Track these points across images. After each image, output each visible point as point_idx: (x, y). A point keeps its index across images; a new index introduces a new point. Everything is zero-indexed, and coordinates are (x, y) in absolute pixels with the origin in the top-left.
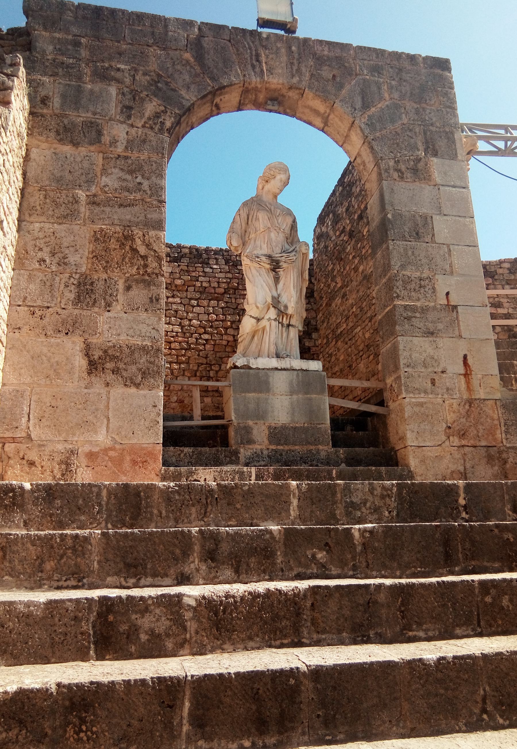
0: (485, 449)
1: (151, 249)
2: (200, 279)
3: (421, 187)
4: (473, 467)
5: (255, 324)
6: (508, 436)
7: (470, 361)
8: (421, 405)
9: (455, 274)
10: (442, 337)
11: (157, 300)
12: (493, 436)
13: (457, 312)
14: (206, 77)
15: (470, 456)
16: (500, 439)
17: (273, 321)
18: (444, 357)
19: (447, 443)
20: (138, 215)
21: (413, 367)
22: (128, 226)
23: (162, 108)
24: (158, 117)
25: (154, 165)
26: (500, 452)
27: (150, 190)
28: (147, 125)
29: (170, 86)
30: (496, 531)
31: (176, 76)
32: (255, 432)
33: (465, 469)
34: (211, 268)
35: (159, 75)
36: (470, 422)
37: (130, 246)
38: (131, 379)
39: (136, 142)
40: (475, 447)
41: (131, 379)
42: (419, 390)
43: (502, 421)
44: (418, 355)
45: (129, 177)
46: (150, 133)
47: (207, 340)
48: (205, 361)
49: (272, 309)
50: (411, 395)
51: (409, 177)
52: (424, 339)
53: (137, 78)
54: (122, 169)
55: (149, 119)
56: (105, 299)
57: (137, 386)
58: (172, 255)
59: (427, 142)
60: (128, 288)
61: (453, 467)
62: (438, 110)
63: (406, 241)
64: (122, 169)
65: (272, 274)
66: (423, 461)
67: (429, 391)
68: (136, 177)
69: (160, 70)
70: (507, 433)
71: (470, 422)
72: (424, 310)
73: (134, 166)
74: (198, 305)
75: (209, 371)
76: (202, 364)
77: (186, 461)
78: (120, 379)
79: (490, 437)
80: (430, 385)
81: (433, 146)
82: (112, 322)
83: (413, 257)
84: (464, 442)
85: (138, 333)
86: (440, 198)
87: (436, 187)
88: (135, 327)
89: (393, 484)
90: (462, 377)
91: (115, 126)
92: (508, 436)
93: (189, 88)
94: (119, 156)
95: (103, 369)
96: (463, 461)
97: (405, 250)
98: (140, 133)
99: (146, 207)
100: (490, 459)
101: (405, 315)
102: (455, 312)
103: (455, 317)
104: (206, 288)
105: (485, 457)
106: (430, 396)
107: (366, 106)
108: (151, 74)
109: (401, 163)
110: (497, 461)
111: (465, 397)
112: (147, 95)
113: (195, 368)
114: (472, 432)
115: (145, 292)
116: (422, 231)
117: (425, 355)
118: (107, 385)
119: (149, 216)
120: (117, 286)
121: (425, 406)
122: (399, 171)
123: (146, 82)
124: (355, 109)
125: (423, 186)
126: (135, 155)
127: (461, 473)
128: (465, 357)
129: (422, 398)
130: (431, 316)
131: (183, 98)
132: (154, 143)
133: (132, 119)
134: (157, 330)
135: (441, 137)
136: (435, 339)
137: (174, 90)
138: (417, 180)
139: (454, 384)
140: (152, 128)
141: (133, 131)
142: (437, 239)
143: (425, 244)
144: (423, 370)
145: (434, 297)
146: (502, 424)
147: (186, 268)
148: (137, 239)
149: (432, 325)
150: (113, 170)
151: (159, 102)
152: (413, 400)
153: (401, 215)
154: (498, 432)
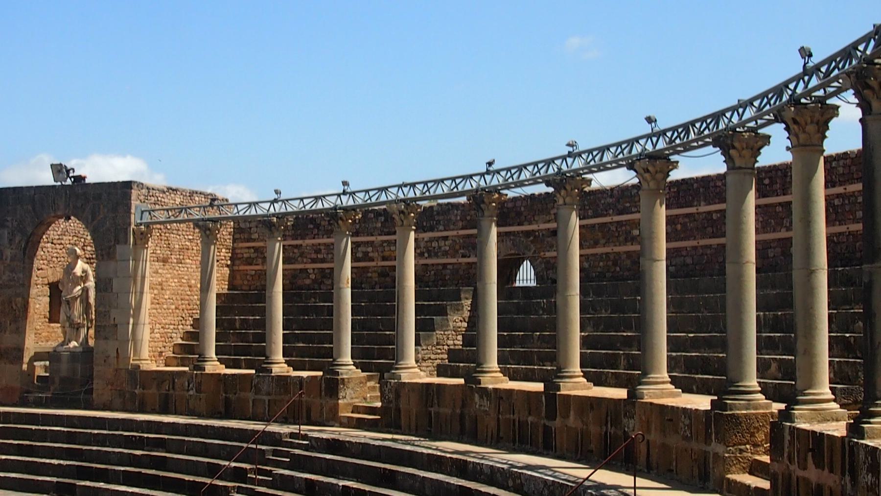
107: (93, 220)
122: (102, 255)
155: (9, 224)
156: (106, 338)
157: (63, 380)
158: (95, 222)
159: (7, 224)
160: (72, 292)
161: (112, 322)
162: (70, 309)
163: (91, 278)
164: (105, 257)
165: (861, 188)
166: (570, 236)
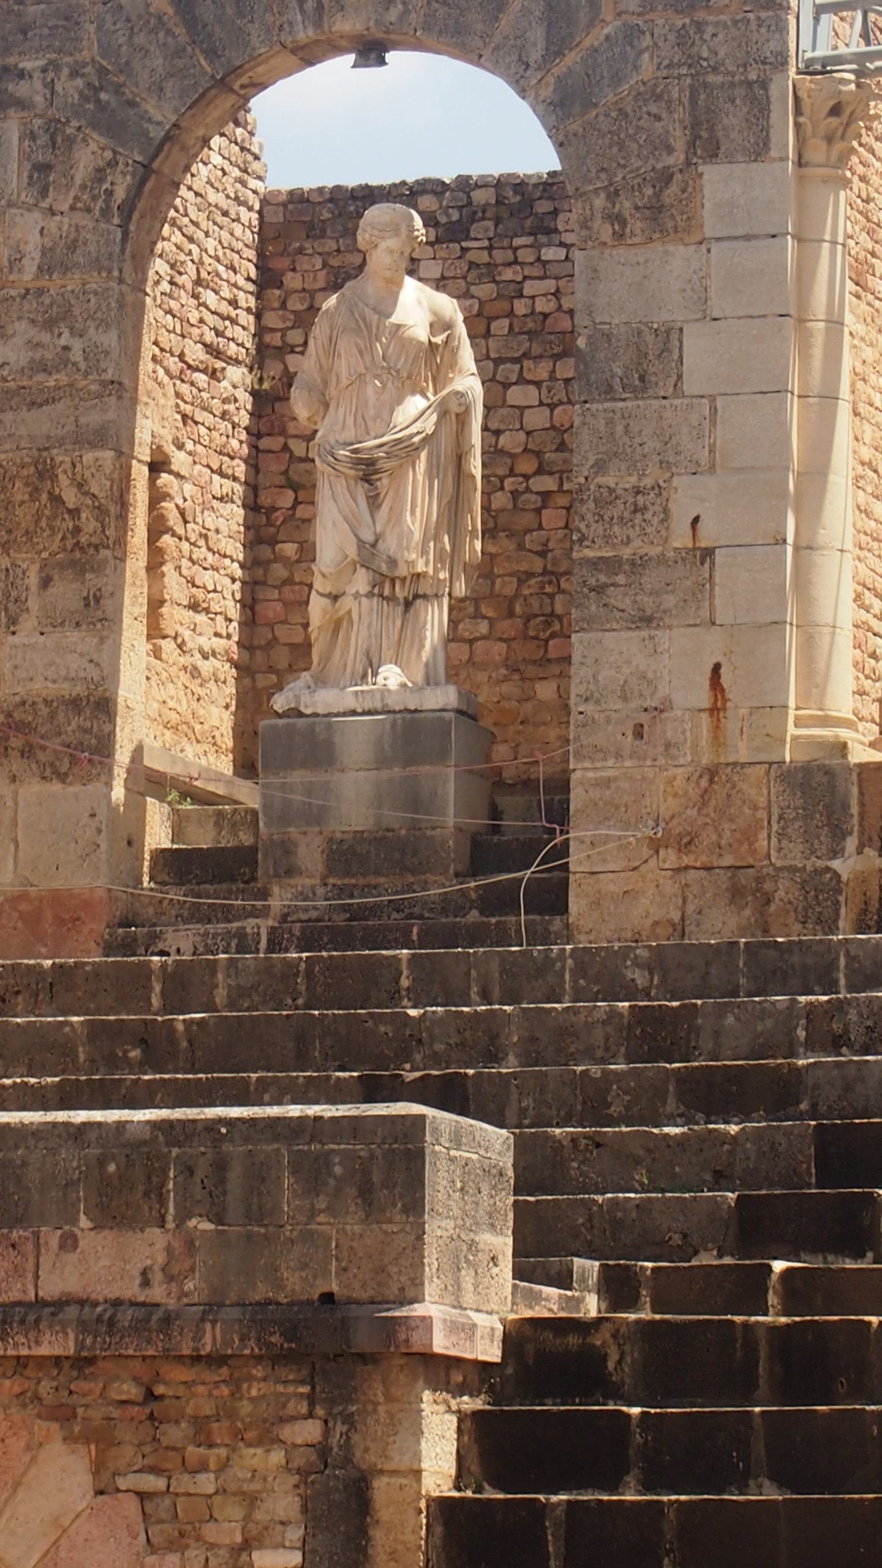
0: (729, 874)
1: (86, 494)
2: (529, 288)
3: (666, 252)
4: (700, 913)
5: (330, 607)
6: (785, 843)
7: (726, 679)
8: (607, 782)
9: (719, 471)
10: (670, 627)
11: (97, 600)
12: (751, 844)
13: (713, 563)
14: (198, 52)
15: (696, 889)
16: (765, 851)
17: (364, 599)
18: (670, 672)
19: (652, 863)
20: (62, 421)
21: (598, 702)
22: (46, 449)
23: (108, 155)
24: (101, 180)
25: (93, 300)
26: (760, 880)
27: (86, 359)
28: (79, 205)
29: (123, 94)
30: (371, 1023)
31: (136, 65)
32: (302, 850)
33: (683, 919)
34: (562, 244)
35: (102, 71)
36: (707, 815)
37: (49, 493)
38: (52, 765)
39: (58, 250)
40: (708, 869)
41: (52, 765)
42: (601, 752)
43: (776, 812)
44: (612, 673)
45: (45, 337)
46: (83, 223)
47: (546, 495)
48: (538, 565)
49: (362, 573)
50: (588, 764)
51: (638, 231)
52: (631, 634)
53: (58, 88)
54: (33, 321)
55: (83, 187)
56: (6, 610)
57: (62, 777)
58: (443, 220)
59: (695, 125)
60: (46, 583)
61: (657, 914)
62: (735, 22)
63: (614, 400)
64: (33, 321)
65: (361, 490)
66: (596, 904)
67: (626, 753)
68: (60, 334)
69: (103, 58)
70: (781, 836)
71: (707, 815)
72: (638, 565)
73: (55, 308)
74: (521, 380)
75: (551, 596)
76: (530, 575)
77: (173, 913)
78: (34, 766)
79: (745, 847)
80: (630, 738)
81: (711, 130)
82: (20, 655)
83: (626, 439)
84: (686, 860)
85: (63, 673)
86: (708, 275)
87: (704, 248)
88: (58, 661)
89: (301, 958)
90: (705, 716)
91: (18, 219)
92: (785, 843)
93: (161, 90)
94: (28, 290)
95: (6, 749)
96: (680, 901)
97: (610, 422)
98: (65, 228)
99: (77, 400)
100: (736, 893)
101: (592, 582)
102: (707, 565)
103: (707, 575)
104: (546, 316)
105: (727, 889)
106: (628, 764)
107: (555, 51)
108: (86, 70)
109: (622, 198)
110: (750, 898)
111: (705, 761)
112: (79, 128)
113: (510, 591)
114: (709, 837)
115: (75, 586)
116: (653, 370)
117: (626, 671)
118: (13, 779)
119: (83, 420)
120: (26, 581)
121: (613, 785)
122: (617, 219)
123: (76, 96)
124: (528, 66)
125: (671, 248)
126: (55, 284)
127: (674, 925)
128: (717, 667)
129: (609, 769)
130: (650, 579)
131: (150, 120)
132: (92, 247)
133: (51, 194)
134: (98, 665)
135: (733, 101)
136: (653, 632)
137: (131, 104)
138: (656, 236)
139: (683, 732)
140: (88, 210)
141: (53, 224)
142: (688, 387)
143: (656, 404)
144: (619, 706)
145: (664, 533)
146: (775, 817)
147: (484, 257)
148: (62, 477)
149: (651, 599)
150: (17, 325)
151: (103, 141)
152: (590, 774)
153: (608, 336)
154: (764, 834)
155: (32, 90)
156: (646, 620)
157: (345, 856)
158: (572, 58)
159: (21, 89)
160: (388, 425)
161: (681, 539)
162: (374, 502)
163: (467, 355)
164: (636, 225)
165: (494, 1142)
166: (821, 665)
